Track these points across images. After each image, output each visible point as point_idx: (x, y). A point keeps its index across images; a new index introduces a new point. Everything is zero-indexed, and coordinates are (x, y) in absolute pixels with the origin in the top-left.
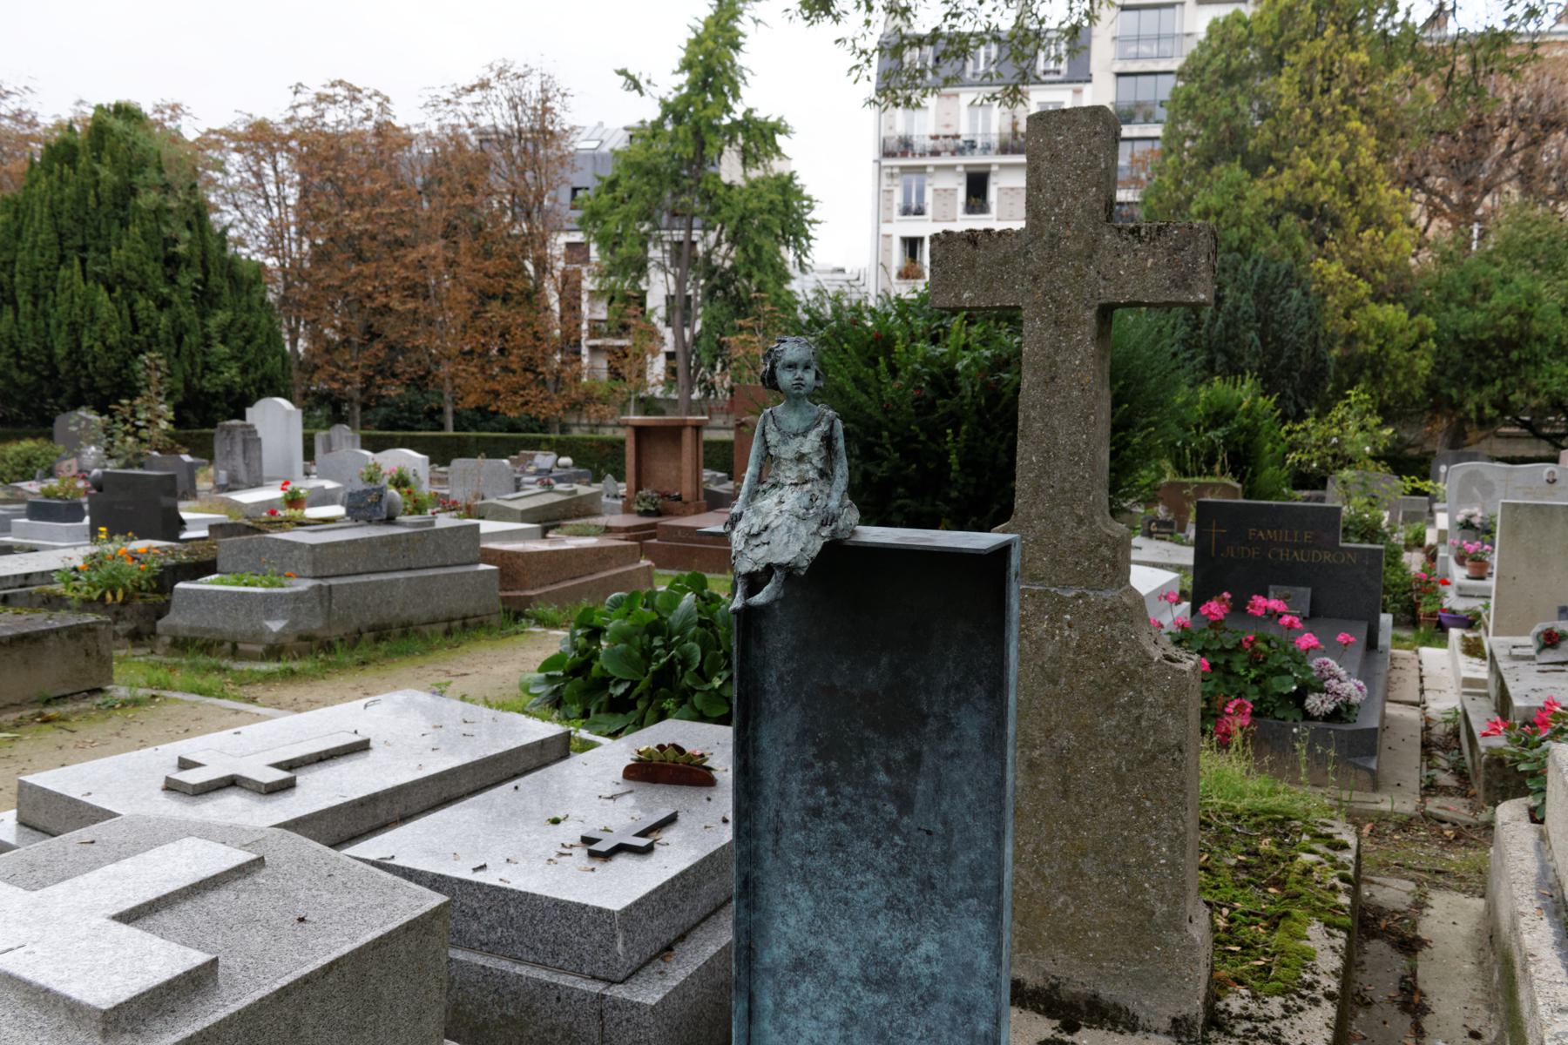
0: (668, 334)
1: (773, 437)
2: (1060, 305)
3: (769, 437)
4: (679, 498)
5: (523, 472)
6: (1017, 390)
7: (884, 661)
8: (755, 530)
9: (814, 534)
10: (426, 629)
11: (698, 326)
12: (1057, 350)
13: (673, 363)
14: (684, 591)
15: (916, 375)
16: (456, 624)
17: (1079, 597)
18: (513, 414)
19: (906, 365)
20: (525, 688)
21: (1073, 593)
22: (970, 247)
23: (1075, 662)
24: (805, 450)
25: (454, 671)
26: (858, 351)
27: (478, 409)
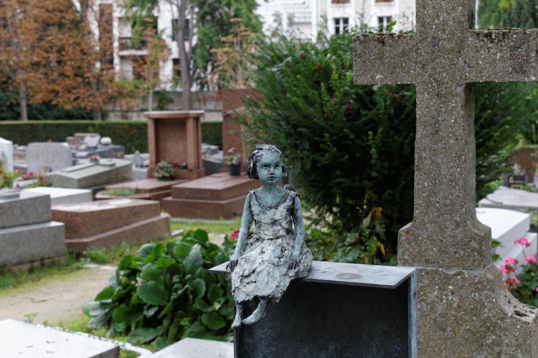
0: (174, 46)
1: (256, 209)
2: (440, 84)
3: (253, 209)
4: (186, 167)
5: (77, 149)
6: (414, 104)
7: (331, 347)
8: (246, 273)
9: (285, 275)
10: (16, 269)
11: (195, 41)
12: (439, 113)
13: (177, 68)
14: (193, 243)
15: (346, 94)
16: (37, 264)
17: (458, 274)
18: (68, 107)
19: (340, 88)
20: (86, 312)
21: (454, 272)
22: (380, 45)
23: (456, 317)
24: (277, 217)
25: (37, 298)
26: (306, 77)
27: (44, 103)
